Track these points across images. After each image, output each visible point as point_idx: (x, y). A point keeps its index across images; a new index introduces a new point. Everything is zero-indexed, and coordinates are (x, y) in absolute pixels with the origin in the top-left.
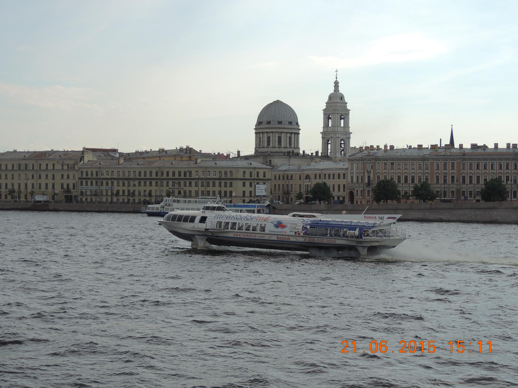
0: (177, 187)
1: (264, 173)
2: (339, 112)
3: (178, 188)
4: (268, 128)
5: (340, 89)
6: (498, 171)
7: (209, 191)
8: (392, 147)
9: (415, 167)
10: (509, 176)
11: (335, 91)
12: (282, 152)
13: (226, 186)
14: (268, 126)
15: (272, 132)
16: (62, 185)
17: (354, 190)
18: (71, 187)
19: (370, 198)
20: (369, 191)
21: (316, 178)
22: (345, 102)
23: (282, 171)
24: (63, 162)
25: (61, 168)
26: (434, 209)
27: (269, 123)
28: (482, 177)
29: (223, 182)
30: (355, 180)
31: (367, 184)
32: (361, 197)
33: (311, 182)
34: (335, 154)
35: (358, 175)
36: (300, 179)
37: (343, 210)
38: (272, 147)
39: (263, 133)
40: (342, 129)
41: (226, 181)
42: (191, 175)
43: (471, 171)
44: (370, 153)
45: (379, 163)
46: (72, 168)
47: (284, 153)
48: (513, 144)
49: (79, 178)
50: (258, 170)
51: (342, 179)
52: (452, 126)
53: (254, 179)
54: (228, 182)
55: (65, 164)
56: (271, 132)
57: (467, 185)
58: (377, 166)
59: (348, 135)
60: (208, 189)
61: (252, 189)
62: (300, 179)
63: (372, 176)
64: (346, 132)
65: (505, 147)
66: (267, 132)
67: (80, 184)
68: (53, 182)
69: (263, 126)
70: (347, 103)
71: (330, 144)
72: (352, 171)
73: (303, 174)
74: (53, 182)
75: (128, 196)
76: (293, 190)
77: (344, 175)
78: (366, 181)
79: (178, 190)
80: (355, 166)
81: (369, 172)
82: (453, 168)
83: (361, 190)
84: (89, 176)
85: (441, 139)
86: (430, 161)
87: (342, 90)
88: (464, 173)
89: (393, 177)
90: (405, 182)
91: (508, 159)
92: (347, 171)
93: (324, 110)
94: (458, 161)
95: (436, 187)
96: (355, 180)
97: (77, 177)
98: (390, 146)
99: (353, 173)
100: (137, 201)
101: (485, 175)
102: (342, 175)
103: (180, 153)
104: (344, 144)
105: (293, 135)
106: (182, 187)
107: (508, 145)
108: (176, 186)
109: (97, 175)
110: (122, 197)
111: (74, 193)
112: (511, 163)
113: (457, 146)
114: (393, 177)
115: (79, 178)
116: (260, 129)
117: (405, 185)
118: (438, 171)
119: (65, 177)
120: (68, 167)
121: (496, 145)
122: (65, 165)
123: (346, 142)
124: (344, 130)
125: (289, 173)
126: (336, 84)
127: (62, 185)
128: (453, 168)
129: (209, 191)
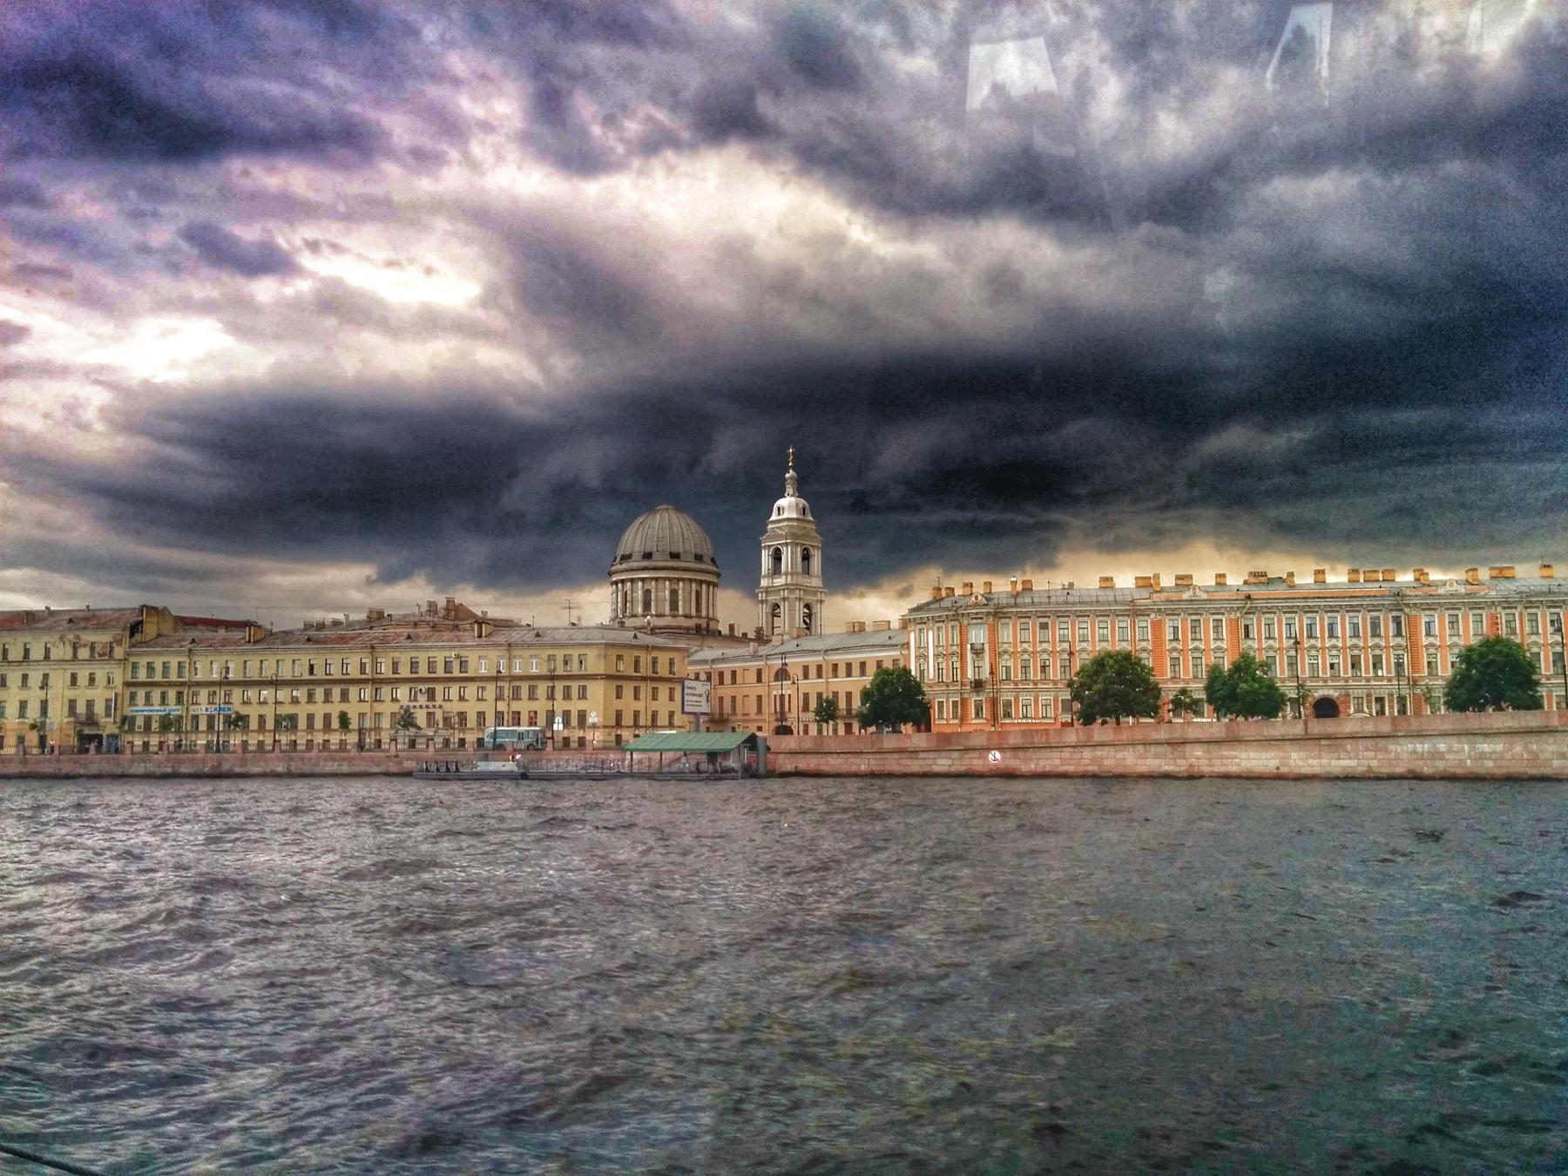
0: (424, 704)
1: (672, 662)
3: (427, 707)
4: (645, 569)
7: (519, 713)
12: (680, 628)
13: (567, 696)
14: (646, 563)
15: (657, 579)
16: (72, 704)
18: (99, 709)
21: (806, 677)
23: (705, 662)
24: (78, 637)
25: (69, 656)
26: (1320, 739)
27: (648, 556)
29: (559, 686)
32: (957, 721)
36: (759, 680)
37: (989, 749)
38: (657, 616)
39: (632, 581)
41: (567, 683)
42: (466, 667)
46: (104, 655)
47: (688, 629)
49: (127, 684)
50: (655, 654)
53: (644, 679)
54: (575, 685)
55: (83, 642)
56: (652, 579)
60: (516, 706)
61: (618, 704)
62: (759, 680)
66: (643, 580)
67: (127, 702)
68: (42, 694)
69: (635, 565)
74: (42, 694)
75: (275, 731)
76: (739, 711)
79: (425, 710)
84: (158, 677)
86: (1153, 616)
91: (1375, 608)
94: (1232, 616)
97: (118, 679)
100: (302, 742)
103: (428, 618)
105: (704, 587)
106: (437, 704)
108: (422, 699)
109: (180, 675)
110: (255, 735)
111: (109, 727)
112: (1386, 619)
115: (127, 684)
116: (626, 571)
118: (1174, 644)
119: (83, 679)
120: (92, 655)
122: (85, 645)
127: (72, 704)
129: (519, 713)
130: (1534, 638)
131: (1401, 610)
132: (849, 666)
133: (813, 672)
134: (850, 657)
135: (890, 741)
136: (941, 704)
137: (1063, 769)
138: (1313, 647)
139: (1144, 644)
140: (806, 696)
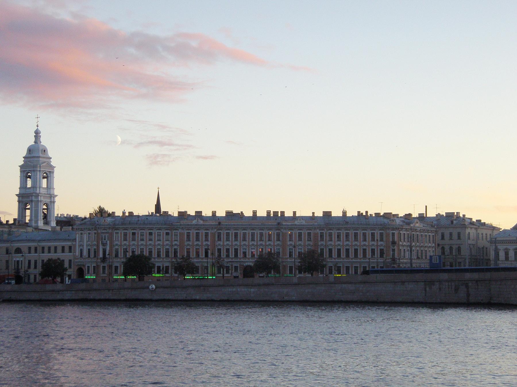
2: (41, 169)
5: (42, 139)
6: (370, 242)
8: (131, 213)
9: (145, 238)
10: (366, 249)
11: (35, 142)
17: (84, 266)
19: (106, 275)
20: (104, 268)
21: (30, 252)
22: (48, 157)
28: (240, 250)
30: (85, 253)
31: (102, 259)
33: (24, 257)
34: (37, 222)
35: (89, 247)
40: (44, 190)
43: (253, 242)
44: (106, 221)
45: (117, 233)
48: (273, 212)
51: (33, 254)
52: (158, 188)
57: (163, 259)
58: (114, 237)
59: (52, 198)
63: (108, 248)
64: (50, 194)
65: (265, 215)
70: (51, 158)
71: (28, 209)
72: (81, 243)
73: (39, 246)
77: (70, 248)
78: (101, 255)
80: (85, 237)
81: (104, 244)
82: (207, 240)
83: (94, 267)
85: (426, 206)
87: (44, 141)
88: (331, 245)
89: (135, 250)
90: (329, 257)
92: (75, 243)
93: (21, 167)
95: (158, 262)
96: (85, 253)
98: (129, 213)
99: (83, 246)
101: (245, 247)
102: (68, 248)
104: (47, 209)
107: (269, 212)
113: (369, 214)
114: (135, 250)
117: (166, 259)
121: (255, 212)
123: (50, 207)
124: (48, 192)
125: (53, 244)
126: (37, 134)
128: (207, 240)
130: (330, 242)
131: (279, 230)
132: (49, 248)
133: (33, 250)
134: (63, 244)
135: (49, 287)
136: (88, 267)
137: (112, 298)
138: (253, 245)
139: (176, 242)
140: (29, 262)
